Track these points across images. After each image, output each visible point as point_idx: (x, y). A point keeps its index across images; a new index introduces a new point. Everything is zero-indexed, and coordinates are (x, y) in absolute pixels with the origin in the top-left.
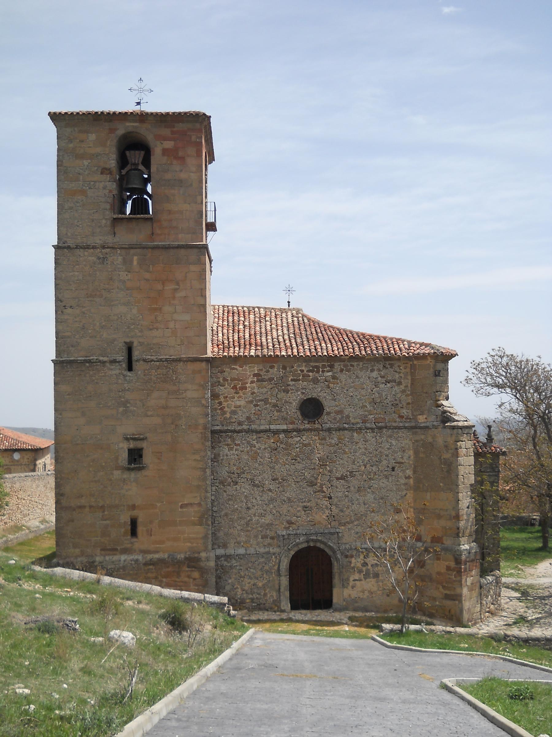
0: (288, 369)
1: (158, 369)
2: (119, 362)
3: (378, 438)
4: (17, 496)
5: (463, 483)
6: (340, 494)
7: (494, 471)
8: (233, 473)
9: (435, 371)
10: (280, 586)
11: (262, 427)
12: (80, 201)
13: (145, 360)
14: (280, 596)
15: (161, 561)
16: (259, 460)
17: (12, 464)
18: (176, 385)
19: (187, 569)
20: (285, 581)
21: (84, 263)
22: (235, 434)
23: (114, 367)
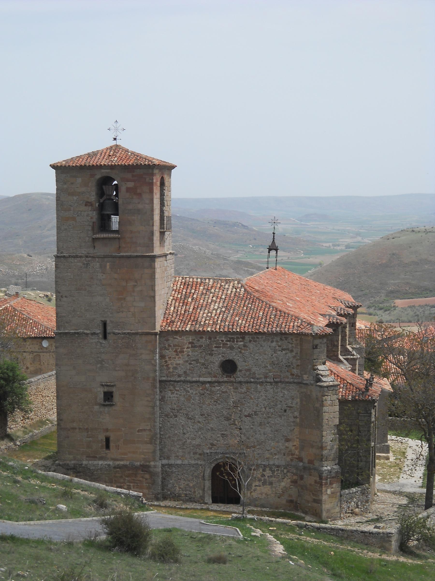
0: (212, 339)
1: (123, 339)
2: (97, 334)
3: (275, 389)
4: (41, 395)
5: (328, 424)
6: (247, 427)
7: (367, 413)
8: (174, 410)
9: (313, 345)
10: (204, 487)
11: (194, 379)
12: (71, 225)
13: (114, 333)
14: (204, 493)
15: (125, 466)
16: (192, 401)
17: (40, 351)
18: (134, 350)
19: (142, 472)
20: (208, 484)
21: (74, 267)
22: (176, 383)
23: (94, 337)
